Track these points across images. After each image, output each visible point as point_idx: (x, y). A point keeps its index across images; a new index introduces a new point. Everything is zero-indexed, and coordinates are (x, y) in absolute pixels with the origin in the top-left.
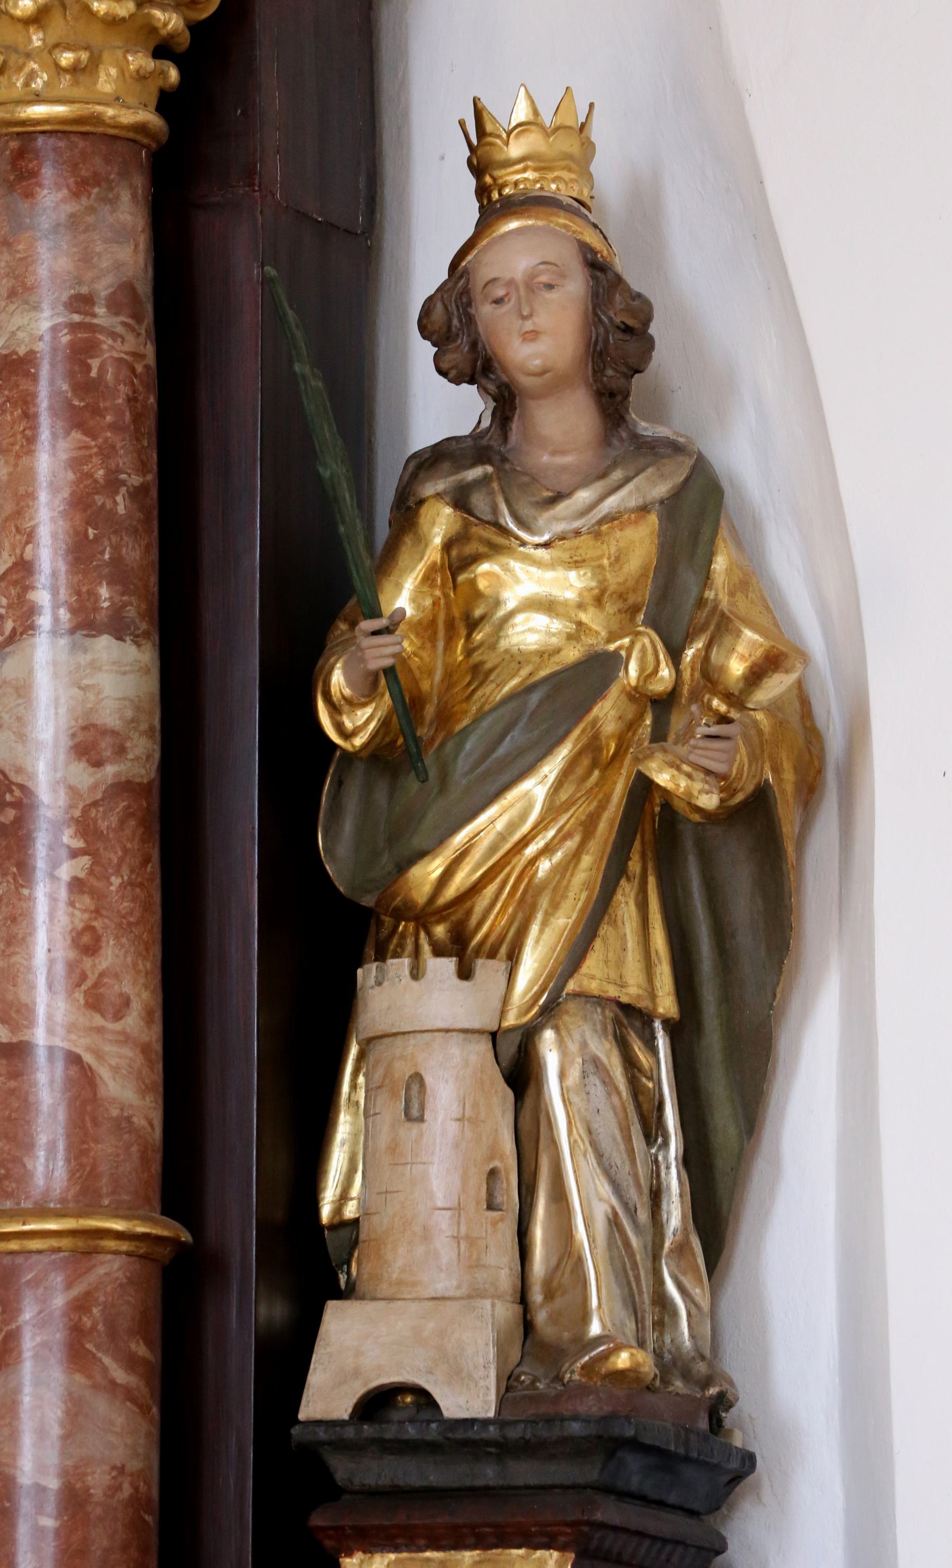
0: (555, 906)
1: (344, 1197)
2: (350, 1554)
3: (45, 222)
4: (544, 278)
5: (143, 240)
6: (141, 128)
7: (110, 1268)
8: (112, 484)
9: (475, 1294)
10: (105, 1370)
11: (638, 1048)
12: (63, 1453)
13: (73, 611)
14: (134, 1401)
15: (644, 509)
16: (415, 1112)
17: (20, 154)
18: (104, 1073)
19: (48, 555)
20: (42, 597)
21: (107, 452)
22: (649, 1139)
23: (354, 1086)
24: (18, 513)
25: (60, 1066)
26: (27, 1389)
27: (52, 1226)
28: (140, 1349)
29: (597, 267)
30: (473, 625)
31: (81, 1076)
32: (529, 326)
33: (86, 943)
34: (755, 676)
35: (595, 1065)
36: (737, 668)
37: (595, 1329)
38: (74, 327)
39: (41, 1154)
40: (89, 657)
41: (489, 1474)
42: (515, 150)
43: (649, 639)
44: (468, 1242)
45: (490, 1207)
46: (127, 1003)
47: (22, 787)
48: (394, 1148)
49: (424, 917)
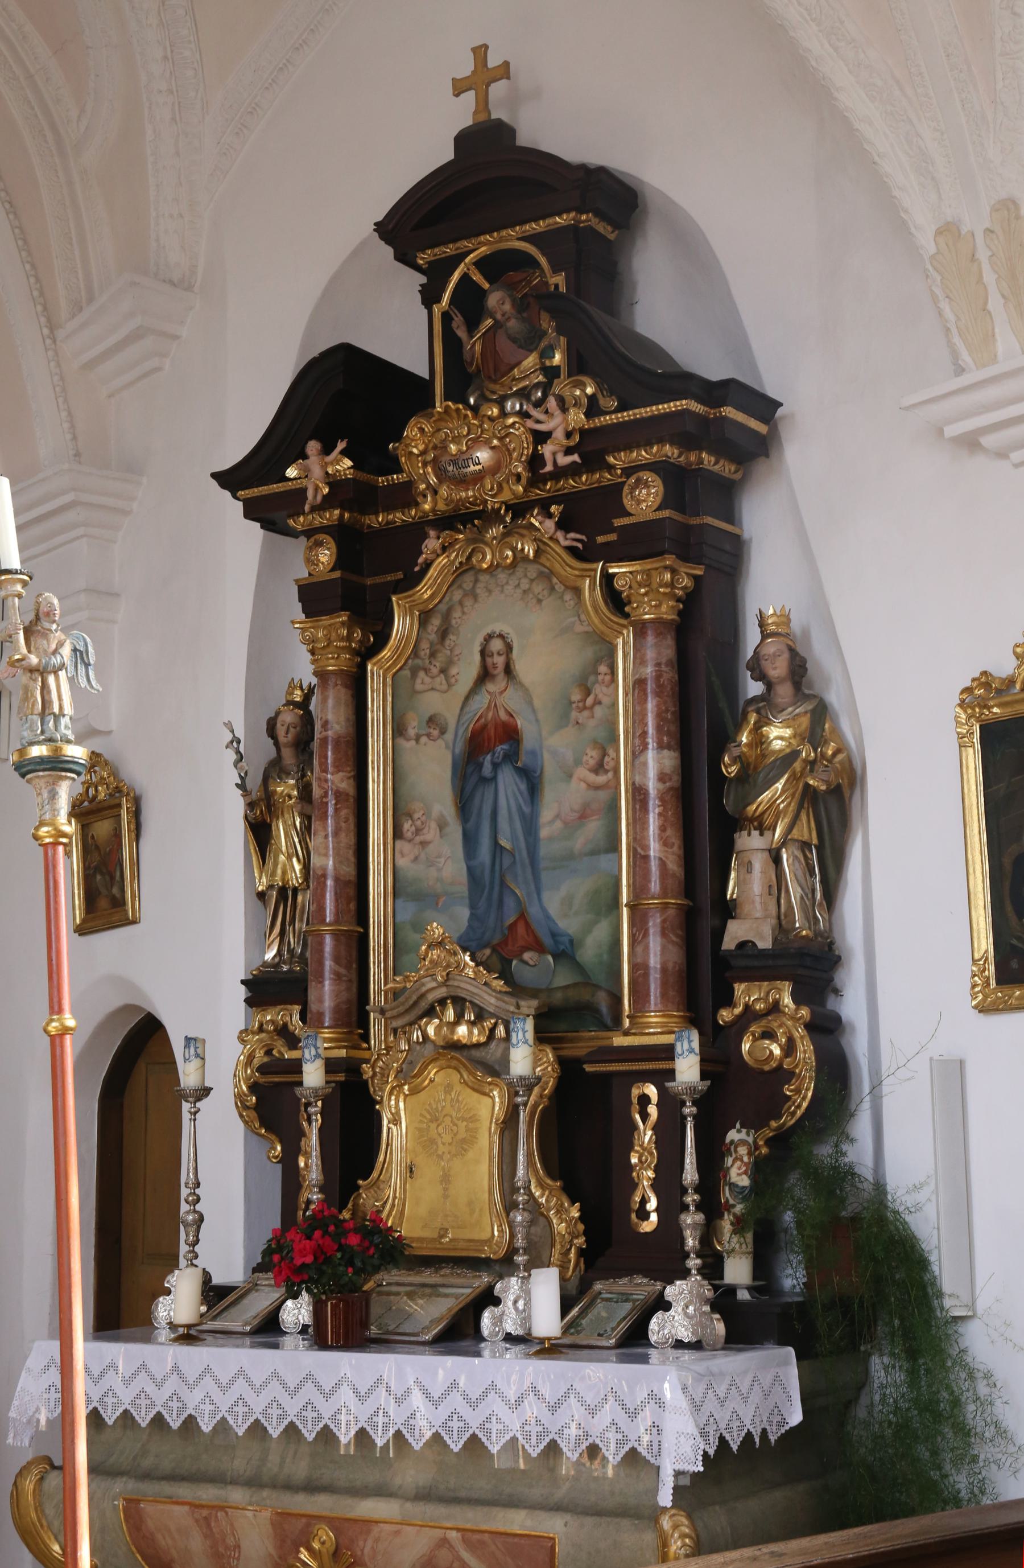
0: (785, 816)
1: (733, 893)
3: (649, 645)
5: (674, 648)
6: (672, 620)
7: (671, 912)
8: (667, 711)
9: (766, 917)
11: (808, 853)
15: (806, 712)
17: (642, 628)
19: (651, 730)
20: (650, 740)
22: (811, 876)
28: (680, 932)
29: (792, 650)
30: (762, 744)
31: (662, 864)
33: (662, 829)
34: (834, 755)
35: (796, 857)
36: (830, 752)
37: (797, 925)
41: (770, 962)
42: (770, 621)
43: (808, 746)
44: (764, 904)
49: (751, 820)
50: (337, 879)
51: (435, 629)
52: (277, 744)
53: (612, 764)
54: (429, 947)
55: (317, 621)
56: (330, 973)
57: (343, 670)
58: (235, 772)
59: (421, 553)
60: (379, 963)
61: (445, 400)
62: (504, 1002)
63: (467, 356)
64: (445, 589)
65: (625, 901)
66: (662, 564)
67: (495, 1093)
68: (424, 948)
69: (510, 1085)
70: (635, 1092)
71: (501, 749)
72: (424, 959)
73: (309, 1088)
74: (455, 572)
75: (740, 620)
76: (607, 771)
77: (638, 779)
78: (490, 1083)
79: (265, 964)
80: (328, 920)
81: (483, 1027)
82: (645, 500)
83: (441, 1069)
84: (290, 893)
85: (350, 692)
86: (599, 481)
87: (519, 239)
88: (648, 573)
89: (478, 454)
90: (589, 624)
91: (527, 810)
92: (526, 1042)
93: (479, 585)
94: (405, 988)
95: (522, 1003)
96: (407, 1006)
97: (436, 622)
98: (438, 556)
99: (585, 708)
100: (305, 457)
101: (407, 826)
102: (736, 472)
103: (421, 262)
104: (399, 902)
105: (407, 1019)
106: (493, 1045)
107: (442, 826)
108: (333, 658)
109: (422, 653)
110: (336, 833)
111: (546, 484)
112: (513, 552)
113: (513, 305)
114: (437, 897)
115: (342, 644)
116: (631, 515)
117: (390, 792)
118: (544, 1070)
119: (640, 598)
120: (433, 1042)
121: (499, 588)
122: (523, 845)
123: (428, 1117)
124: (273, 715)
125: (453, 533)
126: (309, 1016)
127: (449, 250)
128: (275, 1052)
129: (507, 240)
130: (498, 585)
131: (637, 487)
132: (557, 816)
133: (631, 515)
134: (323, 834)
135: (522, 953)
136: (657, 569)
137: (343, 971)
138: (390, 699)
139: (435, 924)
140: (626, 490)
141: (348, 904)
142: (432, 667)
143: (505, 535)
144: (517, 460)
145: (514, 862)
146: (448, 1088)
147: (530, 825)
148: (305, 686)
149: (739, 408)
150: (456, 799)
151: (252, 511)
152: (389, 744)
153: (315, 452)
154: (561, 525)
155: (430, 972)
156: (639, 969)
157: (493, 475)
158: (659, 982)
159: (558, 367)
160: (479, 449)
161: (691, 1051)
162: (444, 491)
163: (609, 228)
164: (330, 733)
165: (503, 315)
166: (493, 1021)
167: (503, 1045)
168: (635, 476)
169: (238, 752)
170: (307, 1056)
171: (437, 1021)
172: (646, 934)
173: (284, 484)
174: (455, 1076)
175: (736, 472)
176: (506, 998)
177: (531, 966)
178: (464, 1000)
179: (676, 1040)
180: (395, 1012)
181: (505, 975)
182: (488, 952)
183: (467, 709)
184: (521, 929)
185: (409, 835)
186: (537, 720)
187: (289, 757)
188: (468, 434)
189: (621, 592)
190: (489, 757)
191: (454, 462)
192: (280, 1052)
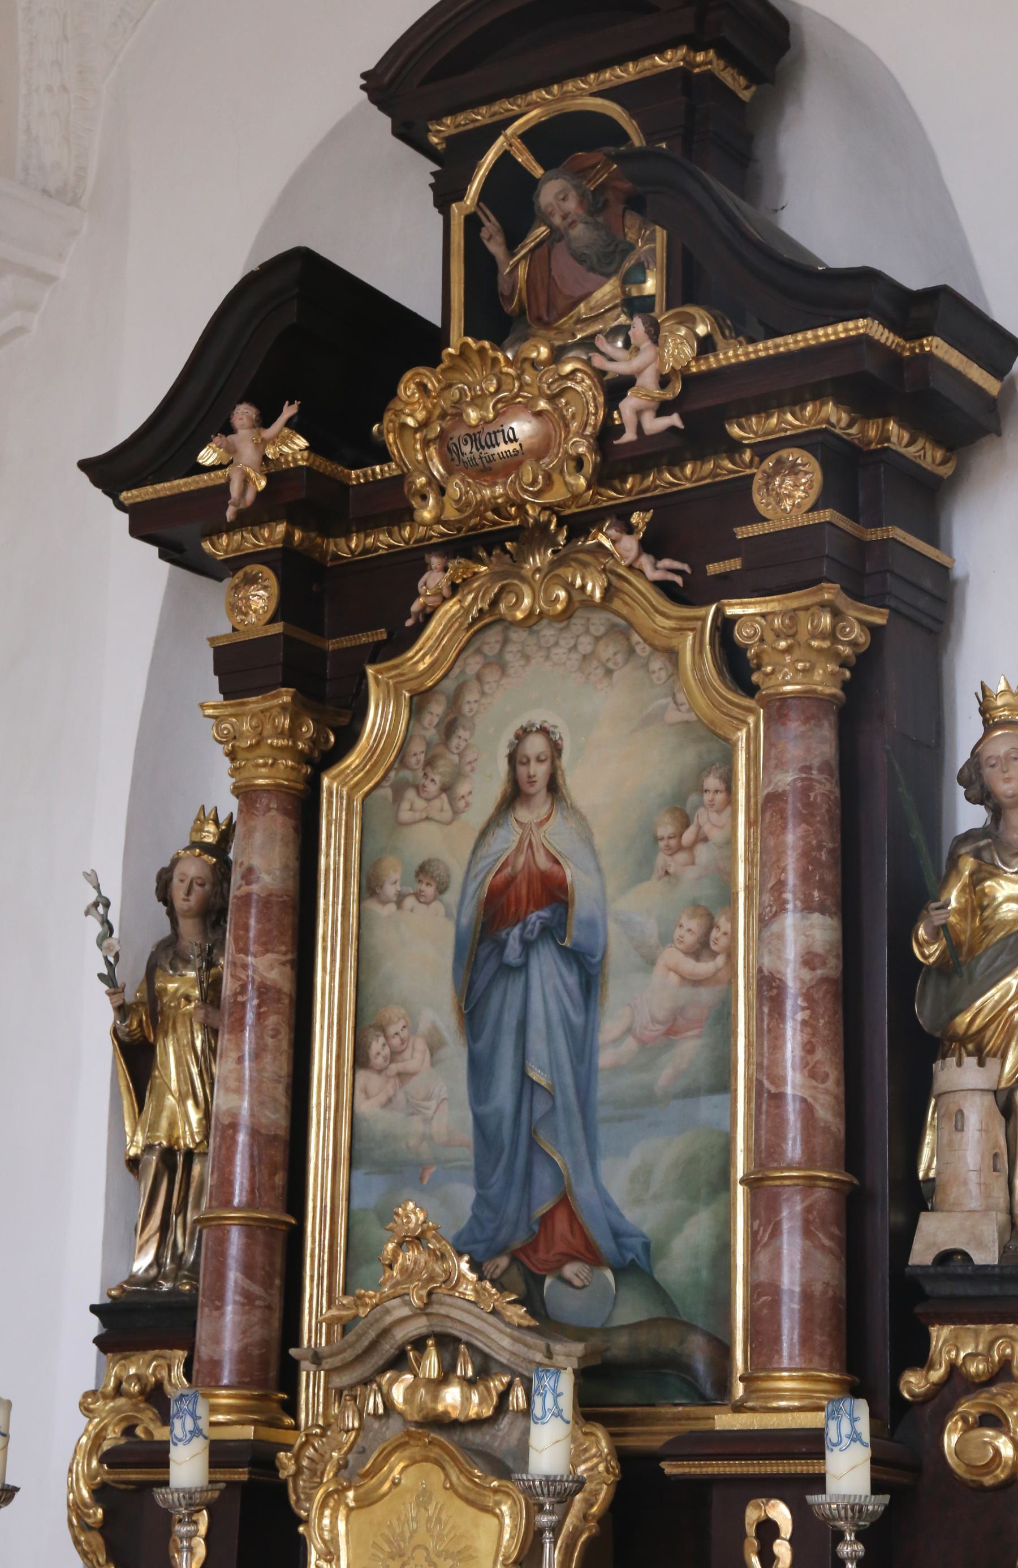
1: (929, 1168)
2: (933, 1326)
4: (1013, 755)
5: (834, 744)
6: (833, 696)
7: (821, 1194)
8: (820, 847)
9: (988, 1209)
10: (819, 1239)
12: (802, 1276)
13: (802, 902)
14: (833, 1254)
16: (959, 1127)
18: (817, 1107)
19: (791, 879)
20: (789, 896)
21: (817, 833)
23: (933, 1118)
24: (778, 860)
26: (785, 1246)
28: (836, 1231)
30: (983, 909)
31: (807, 1111)
32: (1006, 775)
33: (809, 1048)
38: (803, 779)
39: (790, 1142)
40: (809, 922)
41: (996, 1290)
42: (1000, 702)
45: (995, 1170)
46: (827, 1075)
47: (780, 980)
48: (950, 1143)
49: (962, 1040)
50: (254, 1133)
51: (436, 720)
52: (171, 913)
53: (723, 941)
54: (400, 1245)
55: (243, 704)
56: (235, 1293)
57: (282, 785)
58: (99, 955)
59: (417, 595)
60: (320, 1278)
61: (466, 334)
62: (526, 1345)
63: (504, 287)
64: (452, 655)
65: (740, 1174)
66: (816, 599)
67: (505, 1508)
68: (391, 1246)
69: (529, 1491)
70: (752, 1515)
71: (536, 917)
72: (391, 1267)
73: (177, 1490)
74: (471, 625)
75: (946, 708)
76: (714, 955)
77: (767, 962)
78: (496, 1491)
79: (133, 1280)
80: (236, 1201)
81: (488, 1389)
82: (791, 496)
83: (413, 1462)
84: (180, 1159)
85: (290, 823)
86: (713, 474)
87: (593, 95)
88: (792, 614)
89: (514, 425)
90: (691, 709)
91: (577, 1019)
92: (559, 1414)
93: (510, 648)
94: (356, 1317)
95: (557, 1348)
96: (359, 1349)
97: (437, 709)
98: (445, 600)
99: (680, 848)
100: (229, 430)
101: (377, 1047)
102: (944, 462)
103: (435, 140)
104: (359, 1174)
106: (505, 1422)
107: (434, 1046)
108: (265, 765)
109: (413, 760)
110: (257, 1056)
111: (625, 481)
113: (581, 203)
114: (421, 1166)
115: (281, 742)
116: (764, 519)
117: (350, 990)
118: (592, 1469)
119: (777, 658)
120: (401, 1414)
121: (543, 653)
122: (569, 1079)
123: (387, 1549)
124: (167, 864)
125: (471, 564)
126: (196, 1366)
127: (481, 116)
128: (139, 1432)
129: (574, 97)
130: (540, 647)
132: (629, 1030)
133: (764, 519)
134: (234, 1055)
135: (561, 1264)
136: (806, 608)
137: (257, 1289)
138: (357, 835)
139: (411, 1205)
140: (758, 481)
141: (272, 1174)
142: (428, 783)
143: (554, 565)
144: (577, 434)
145: (553, 1108)
146: (424, 1498)
147: (582, 1047)
148: (222, 818)
149: (954, 342)
150: (459, 1002)
151: (145, 524)
152: (354, 908)
153: (245, 421)
155: (400, 1290)
156: (764, 1295)
157: (539, 459)
158: (797, 1317)
159: (652, 297)
160: (515, 417)
161: (855, 1437)
162: (455, 488)
163: (742, 81)
165: (564, 217)
166: (505, 1379)
167: (520, 1423)
168: (774, 457)
169: (105, 922)
171: (409, 1377)
172: (776, 1232)
173: (196, 477)
174: (436, 1476)
175: (944, 462)
176: (530, 1338)
177: (580, 1289)
178: (457, 1340)
179: (828, 1418)
181: (532, 1300)
182: (503, 1262)
183: (483, 851)
184: (561, 1224)
185: (379, 1061)
186: (599, 870)
187: (189, 929)
188: (498, 390)
189: (747, 648)
190: (516, 931)
191: (473, 438)
192: (147, 1431)
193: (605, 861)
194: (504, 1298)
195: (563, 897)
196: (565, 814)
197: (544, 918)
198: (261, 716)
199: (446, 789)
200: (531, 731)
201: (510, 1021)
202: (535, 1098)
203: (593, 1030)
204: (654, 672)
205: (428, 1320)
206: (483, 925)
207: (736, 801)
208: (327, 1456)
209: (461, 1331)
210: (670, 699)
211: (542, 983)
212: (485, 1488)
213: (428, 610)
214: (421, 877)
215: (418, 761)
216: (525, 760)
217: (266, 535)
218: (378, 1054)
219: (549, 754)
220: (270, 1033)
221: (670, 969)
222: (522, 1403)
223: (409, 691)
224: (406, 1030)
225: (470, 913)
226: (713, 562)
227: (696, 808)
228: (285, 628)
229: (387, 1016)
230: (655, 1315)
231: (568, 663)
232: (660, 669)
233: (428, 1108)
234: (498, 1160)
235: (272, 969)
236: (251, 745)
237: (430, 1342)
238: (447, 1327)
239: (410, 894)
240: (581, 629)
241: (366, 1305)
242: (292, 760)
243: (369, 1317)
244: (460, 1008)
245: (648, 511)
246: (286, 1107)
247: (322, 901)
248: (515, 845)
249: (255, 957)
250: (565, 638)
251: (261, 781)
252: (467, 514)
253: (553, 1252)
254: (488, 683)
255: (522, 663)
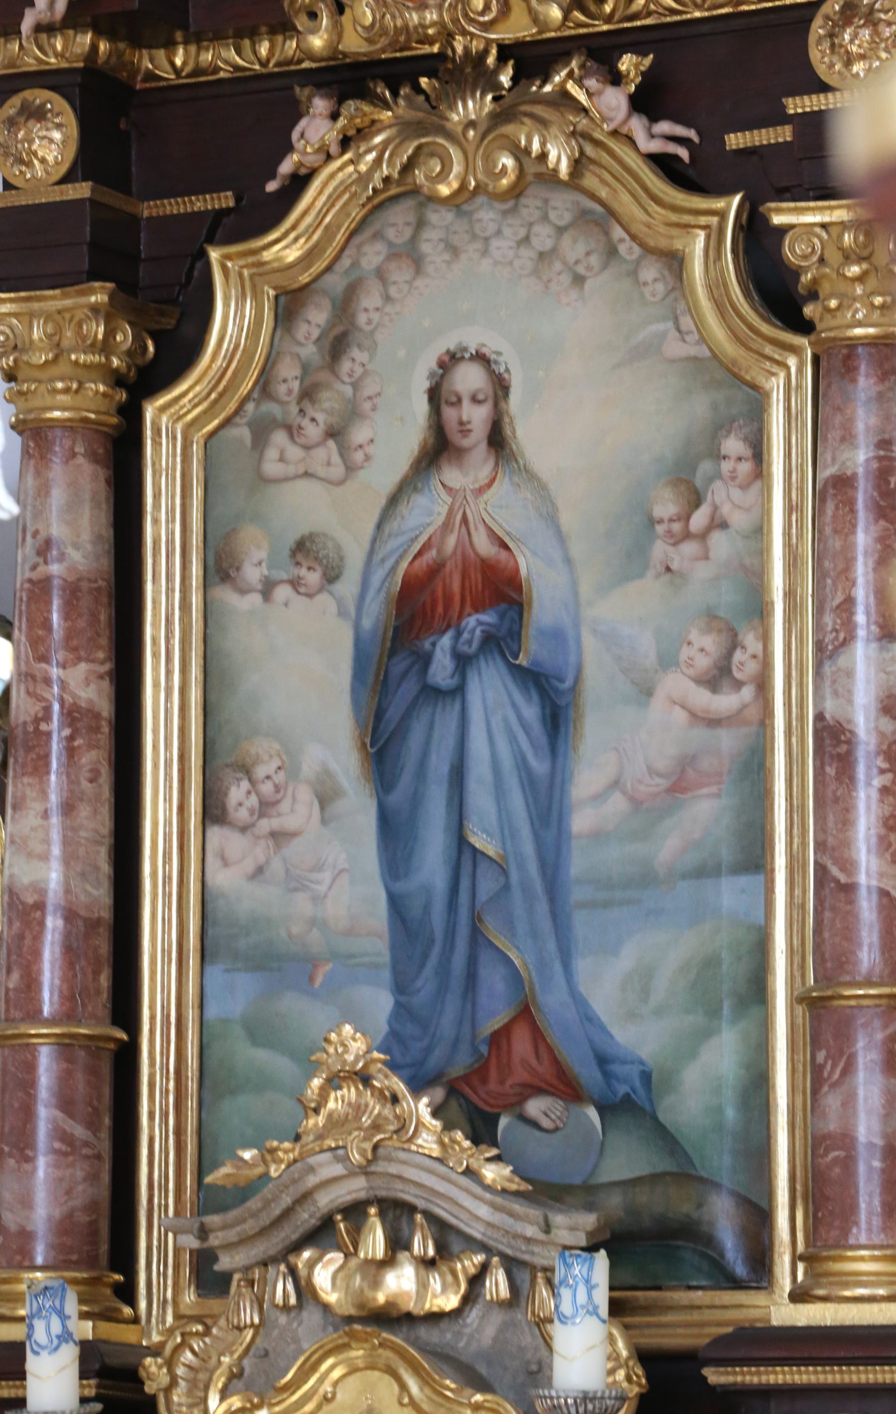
3: (862, 396)
17: (848, 357)
20: (860, 618)
25: (875, 897)
27: (872, 992)
38: (879, 459)
40: (890, 654)
47: (851, 732)
50: (70, 915)
51: (316, 333)
53: (752, 667)
57: (86, 420)
62: (511, 1214)
64: (340, 237)
68: (316, 1082)
71: (476, 623)
72: (316, 1111)
76: (738, 685)
77: (830, 707)
80: (46, 1010)
83: (353, 1370)
85: (102, 474)
91: (540, 766)
95: (559, 1219)
96: (265, 1219)
97: (316, 317)
98: (329, 158)
99: (687, 535)
101: (238, 796)
104: (214, 972)
105: (259, 1250)
106: (473, 1315)
107: (326, 796)
108: (67, 390)
109: (282, 389)
110: (68, 808)
112: (517, 159)
119: (842, 287)
120: (326, 1308)
121: (478, 245)
122: (528, 847)
125: (367, 108)
131: (848, 22)
132: (616, 784)
135: (523, 1099)
137: (79, 1131)
140: (818, 29)
142: (305, 423)
145: (507, 887)
147: (548, 806)
152: (196, 600)
154: (646, 103)
164: (55, 568)
166: (479, 1258)
170: (40, 1334)
172: (849, 1069)
174: (387, 1388)
176: (517, 1207)
178: (412, 1209)
180: (232, 1235)
183: (393, 525)
184: (521, 1044)
185: (242, 815)
186: (568, 561)
190: (446, 641)
193: (576, 549)
194: (482, 1153)
195: (515, 596)
196: (516, 479)
197: (489, 624)
198: (57, 317)
199: (333, 433)
200: (463, 358)
201: (440, 765)
202: (479, 872)
203: (563, 782)
204: (645, 284)
205: (368, 1181)
206: (396, 629)
207: (770, 475)
208: (214, 1360)
209: (416, 1196)
210: (670, 324)
211: (486, 715)
212: (461, 1404)
213: (303, 171)
214: (300, 557)
215: (290, 392)
216: (454, 399)
217: (59, 47)
218: (240, 804)
219: (490, 393)
220: (88, 775)
221: (675, 703)
222: (504, 1292)
223: (275, 288)
224: (282, 774)
225: (375, 612)
226: (735, 131)
227: (710, 480)
228: (93, 190)
229: (253, 751)
230: (660, 1169)
231: (517, 263)
232: (655, 280)
233: (318, 882)
234: (425, 956)
235: (88, 685)
236: (46, 362)
237: (373, 1211)
238: (396, 1190)
239: (282, 581)
240: (537, 214)
241: (280, 1161)
242: (104, 383)
243: (284, 1177)
244: (364, 744)
245: (645, 55)
246: (109, 877)
247: (149, 587)
248: (440, 520)
249: (64, 667)
250: (510, 226)
251: (57, 414)
252: (379, 46)
253: (509, 1082)
254: (394, 283)
255: (447, 257)
